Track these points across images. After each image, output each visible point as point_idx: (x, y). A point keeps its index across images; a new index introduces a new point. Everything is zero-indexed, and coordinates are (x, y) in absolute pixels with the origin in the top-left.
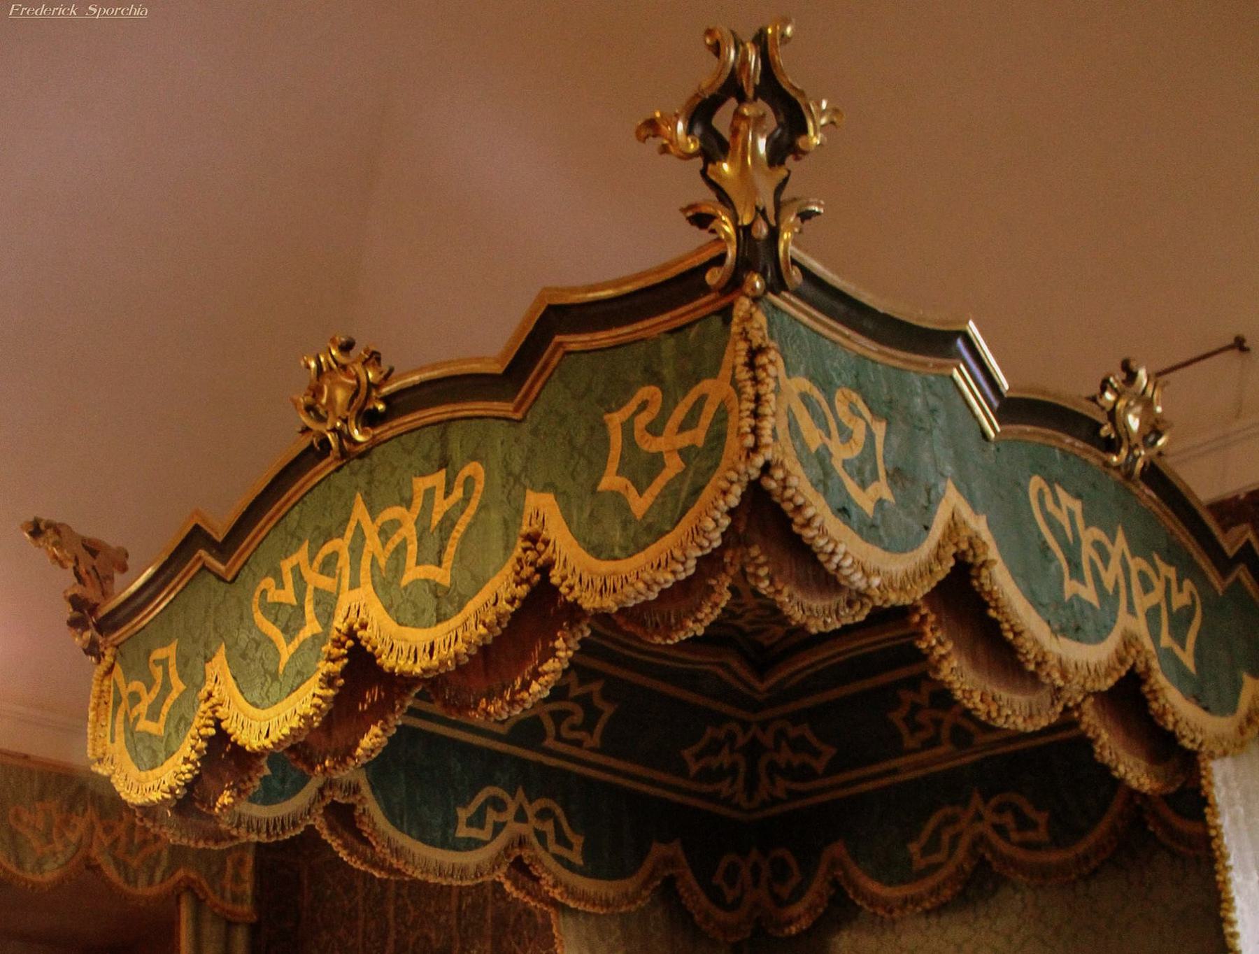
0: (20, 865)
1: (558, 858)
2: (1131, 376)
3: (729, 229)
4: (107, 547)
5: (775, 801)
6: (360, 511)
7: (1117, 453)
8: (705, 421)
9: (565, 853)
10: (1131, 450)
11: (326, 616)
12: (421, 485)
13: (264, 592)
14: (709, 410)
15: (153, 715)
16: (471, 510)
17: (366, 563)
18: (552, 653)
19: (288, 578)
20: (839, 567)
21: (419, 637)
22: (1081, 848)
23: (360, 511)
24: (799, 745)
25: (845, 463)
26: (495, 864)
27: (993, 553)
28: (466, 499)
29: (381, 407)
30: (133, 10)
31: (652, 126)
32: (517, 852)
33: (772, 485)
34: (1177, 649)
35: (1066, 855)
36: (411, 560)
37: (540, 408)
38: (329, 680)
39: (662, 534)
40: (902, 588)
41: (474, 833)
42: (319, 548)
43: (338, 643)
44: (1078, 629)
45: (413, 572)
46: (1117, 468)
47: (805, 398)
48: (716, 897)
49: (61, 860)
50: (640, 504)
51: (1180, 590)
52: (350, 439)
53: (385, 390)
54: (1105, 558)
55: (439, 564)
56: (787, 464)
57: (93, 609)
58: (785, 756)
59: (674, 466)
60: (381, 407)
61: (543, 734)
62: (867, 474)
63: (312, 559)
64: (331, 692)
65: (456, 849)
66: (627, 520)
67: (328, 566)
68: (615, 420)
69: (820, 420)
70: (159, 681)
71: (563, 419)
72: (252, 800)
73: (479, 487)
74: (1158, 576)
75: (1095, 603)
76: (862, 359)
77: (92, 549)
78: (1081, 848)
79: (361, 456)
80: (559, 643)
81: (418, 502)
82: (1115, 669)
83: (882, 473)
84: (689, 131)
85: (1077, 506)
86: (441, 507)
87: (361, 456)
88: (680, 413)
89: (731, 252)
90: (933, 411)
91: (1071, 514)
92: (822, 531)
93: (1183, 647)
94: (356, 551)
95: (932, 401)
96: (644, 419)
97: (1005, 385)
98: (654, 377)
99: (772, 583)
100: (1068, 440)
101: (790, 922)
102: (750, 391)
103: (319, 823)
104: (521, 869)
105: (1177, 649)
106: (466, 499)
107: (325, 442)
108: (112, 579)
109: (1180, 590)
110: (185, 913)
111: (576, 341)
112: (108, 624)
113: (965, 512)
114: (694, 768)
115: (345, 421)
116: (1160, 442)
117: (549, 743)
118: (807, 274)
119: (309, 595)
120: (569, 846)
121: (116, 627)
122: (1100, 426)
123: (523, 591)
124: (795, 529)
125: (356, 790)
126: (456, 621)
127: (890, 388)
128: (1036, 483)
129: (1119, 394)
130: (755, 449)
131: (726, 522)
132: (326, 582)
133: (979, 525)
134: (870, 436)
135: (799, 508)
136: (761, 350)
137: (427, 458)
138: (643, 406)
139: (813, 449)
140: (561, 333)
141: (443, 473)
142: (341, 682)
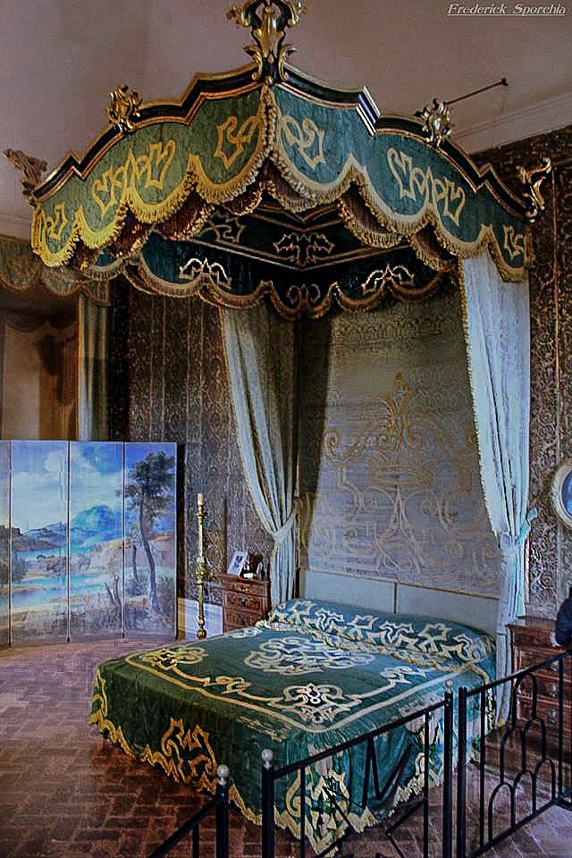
0: (12, 282)
1: (221, 287)
2: (437, 106)
3: (260, 59)
4: (38, 161)
5: (312, 264)
6: (131, 157)
7: (429, 138)
8: (251, 133)
9: (224, 284)
10: (435, 137)
11: (118, 197)
12: (153, 147)
13: (96, 186)
14: (253, 128)
15: (56, 233)
16: (170, 160)
17: (133, 176)
18: (199, 216)
19: (105, 181)
20: (299, 190)
21: (151, 208)
22: (425, 290)
23: (131, 157)
24: (321, 242)
25: (305, 149)
26: (195, 288)
27: (368, 181)
28: (169, 155)
29: (138, 115)
30: (553, 10)
31: (233, 13)
32: (204, 284)
33: (273, 160)
34: (451, 216)
35: (420, 292)
36: (149, 178)
37: (195, 121)
38: (119, 223)
39: (235, 175)
40: (327, 197)
41: (186, 277)
42: (116, 169)
43: (122, 209)
44: (405, 210)
45: (149, 183)
46: (430, 143)
47: (289, 125)
48: (287, 302)
49: (29, 280)
50: (228, 163)
51: (455, 191)
52: (126, 126)
53: (140, 108)
54: (420, 179)
55: (159, 180)
56: (280, 151)
57: (33, 187)
58: (315, 246)
59: (240, 149)
60: (138, 115)
61: (215, 236)
62: (314, 154)
63: (114, 173)
64: (120, 228)
65: (178, 283)
66: (224, 169)
67: (120, 177)
68: (221, 128)
69: (295, 133)
70: (58, 217)
71: (203, 126)
72: (96, 264)
73: (173, 151)
74: (446, 187)
75: (414, 199)
76: (315, 106)
77: (32, 161)
78: (425, 290)
79: (132, 133)
80: (202, 213)
81: (151, 154)
82: (419, 224)
83: (321, 152)
84: (246, 17)
85: (410, 160)
86: (161, 157)
87: (132, 133)
88: (243, 129)
89: (260, 67)
90: (347, 125)
91: (407, 164)
92: (293, 177)
93: (454, 215)
94: (129, 173)
95: (347, 121)
96: (231, 129)
97: (378, 114)
98: (235, 114)
99: (277, 194)
100: (407, 133)
101: (316, 313)
102: (266, 124)
103: (125, 273)
104: (205, 291)
105: (451, 216)
106: (169, 155)
107: (117, 127)
108: (40, 175)
109: (455, 191)
110: (81, 301)
111: (209, 96)
112: (39, 193)
113: (357, 165)
114: (278, 250)
115: (125, 120)
116: (449, 133)
117: (218, 240)
118: (291, 74)
119: (112, 188)
120: (226, 282)
121: (41, 195)
122: (422, 127)
123: (187, 193)
124: (283, 176)
125: (138, 260)
126: (164, 203)
127: (327, 118)
128: (392, 151)
129: (430, 114)
130: (266, 146)
131: (257, 173)
132: (119, 184)
133: (364, 171)
134: (317, 137)
135: (283, 169)
136: (271, 107)
137: (155, 137)
138: (231, 124)
139: (291, 145)
140: (204, 91)
141: (160, 144)
142: (124, 224)
